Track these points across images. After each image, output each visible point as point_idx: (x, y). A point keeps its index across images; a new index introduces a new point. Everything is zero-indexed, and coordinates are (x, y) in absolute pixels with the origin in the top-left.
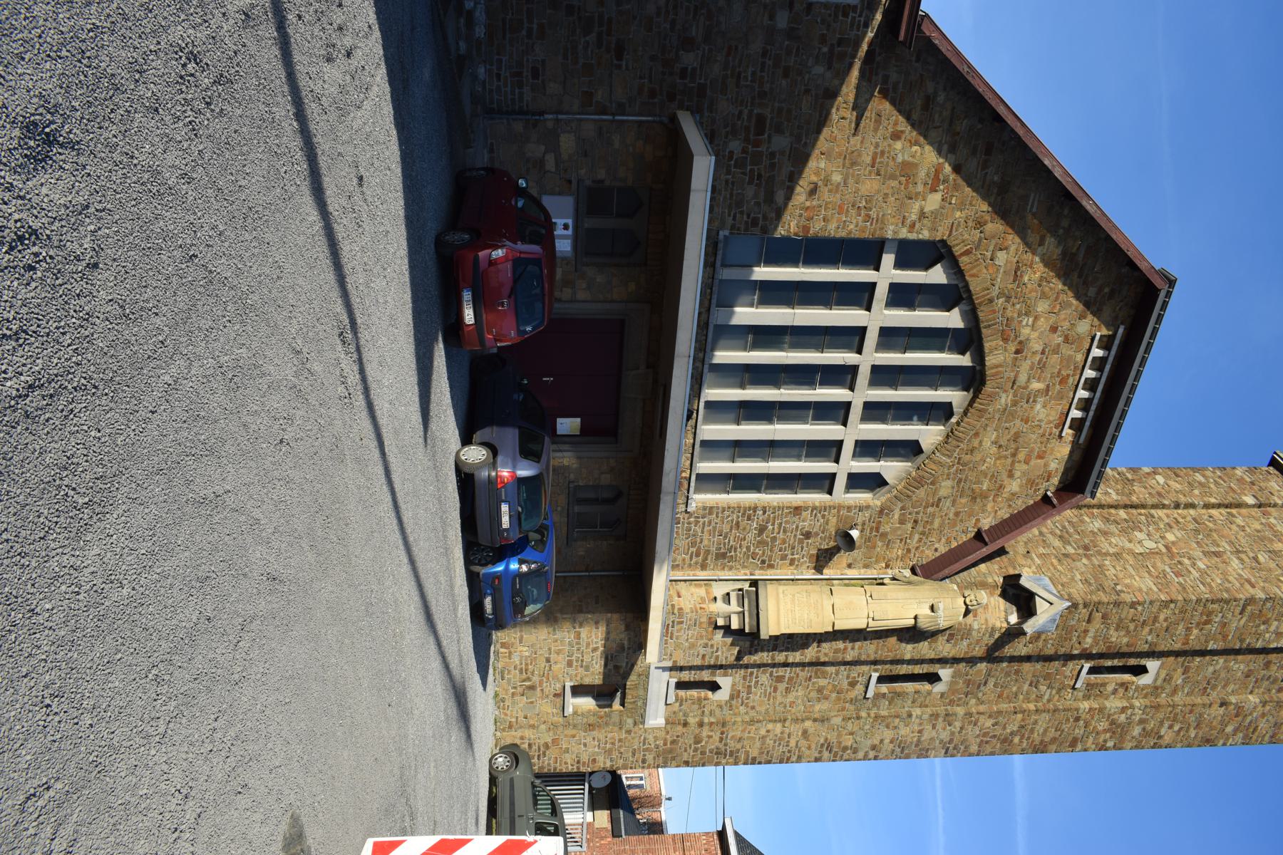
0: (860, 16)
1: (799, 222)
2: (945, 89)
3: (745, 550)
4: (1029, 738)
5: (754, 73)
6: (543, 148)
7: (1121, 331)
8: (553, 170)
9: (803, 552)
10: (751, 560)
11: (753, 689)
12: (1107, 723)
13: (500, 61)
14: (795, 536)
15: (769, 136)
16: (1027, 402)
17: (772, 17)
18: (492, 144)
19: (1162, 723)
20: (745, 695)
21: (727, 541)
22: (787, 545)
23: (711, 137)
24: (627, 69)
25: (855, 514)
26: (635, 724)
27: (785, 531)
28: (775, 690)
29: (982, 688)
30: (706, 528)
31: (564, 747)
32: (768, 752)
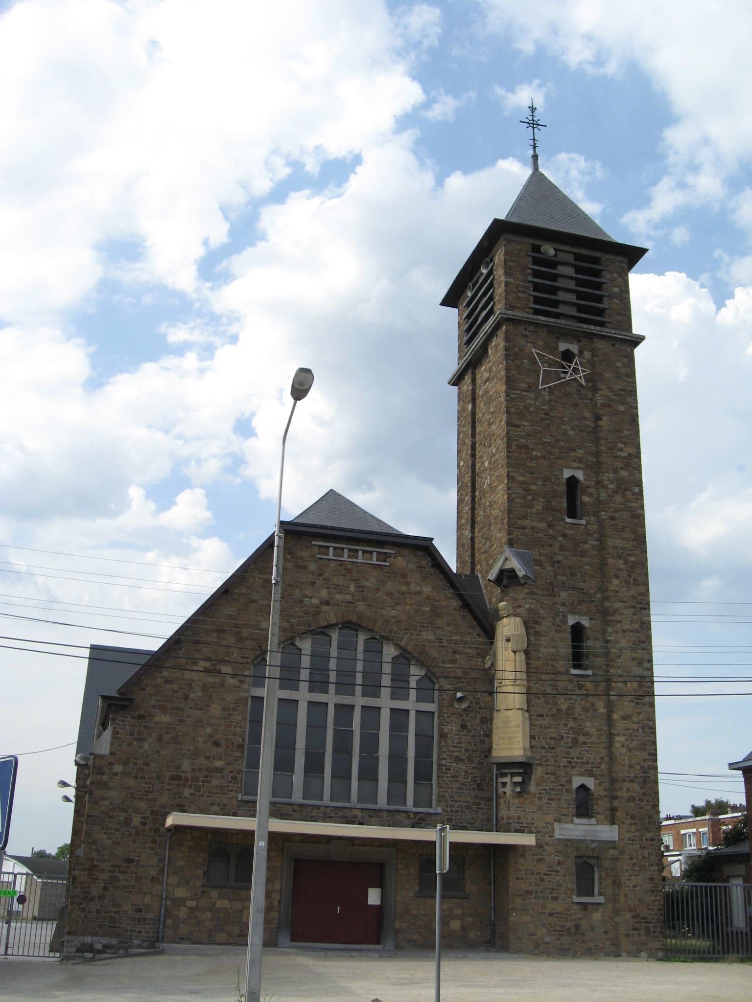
0: (119, 725)
1: (235, 751)
2: (161, 672)
3: (475, 771)
4: (630, 550)
5: (146, 783)
6: (182, 908)
7: (314, 543)
8: (196, 902)
9: (478, 728)
10: (484, 766)
11: (585, 760)
12: (617, 496)
13: (131, 931)
14: (464, 735)
15: (183, 772)
16: (364, 591)
17: (116, 774)
18: (179, 938)
19: (616, 457)
20: (589, 766)
21: (467, 784)
22: (472, 740)
23: (715, 850)
24: (139, 856)
25: (447, 695)
26: (614, 848)
27: (460, 743)
28: (584, 743)
29: (585, 591)
30: (457, 798)
31: (637, 903)
32: (644, 744)
